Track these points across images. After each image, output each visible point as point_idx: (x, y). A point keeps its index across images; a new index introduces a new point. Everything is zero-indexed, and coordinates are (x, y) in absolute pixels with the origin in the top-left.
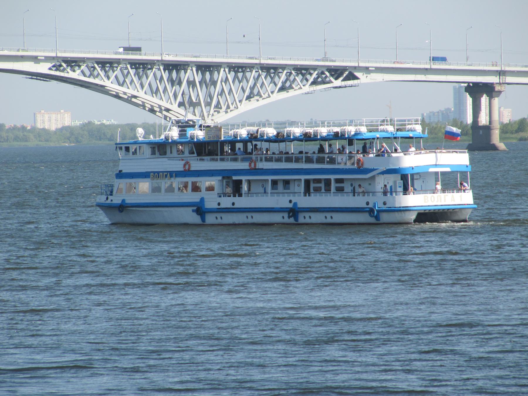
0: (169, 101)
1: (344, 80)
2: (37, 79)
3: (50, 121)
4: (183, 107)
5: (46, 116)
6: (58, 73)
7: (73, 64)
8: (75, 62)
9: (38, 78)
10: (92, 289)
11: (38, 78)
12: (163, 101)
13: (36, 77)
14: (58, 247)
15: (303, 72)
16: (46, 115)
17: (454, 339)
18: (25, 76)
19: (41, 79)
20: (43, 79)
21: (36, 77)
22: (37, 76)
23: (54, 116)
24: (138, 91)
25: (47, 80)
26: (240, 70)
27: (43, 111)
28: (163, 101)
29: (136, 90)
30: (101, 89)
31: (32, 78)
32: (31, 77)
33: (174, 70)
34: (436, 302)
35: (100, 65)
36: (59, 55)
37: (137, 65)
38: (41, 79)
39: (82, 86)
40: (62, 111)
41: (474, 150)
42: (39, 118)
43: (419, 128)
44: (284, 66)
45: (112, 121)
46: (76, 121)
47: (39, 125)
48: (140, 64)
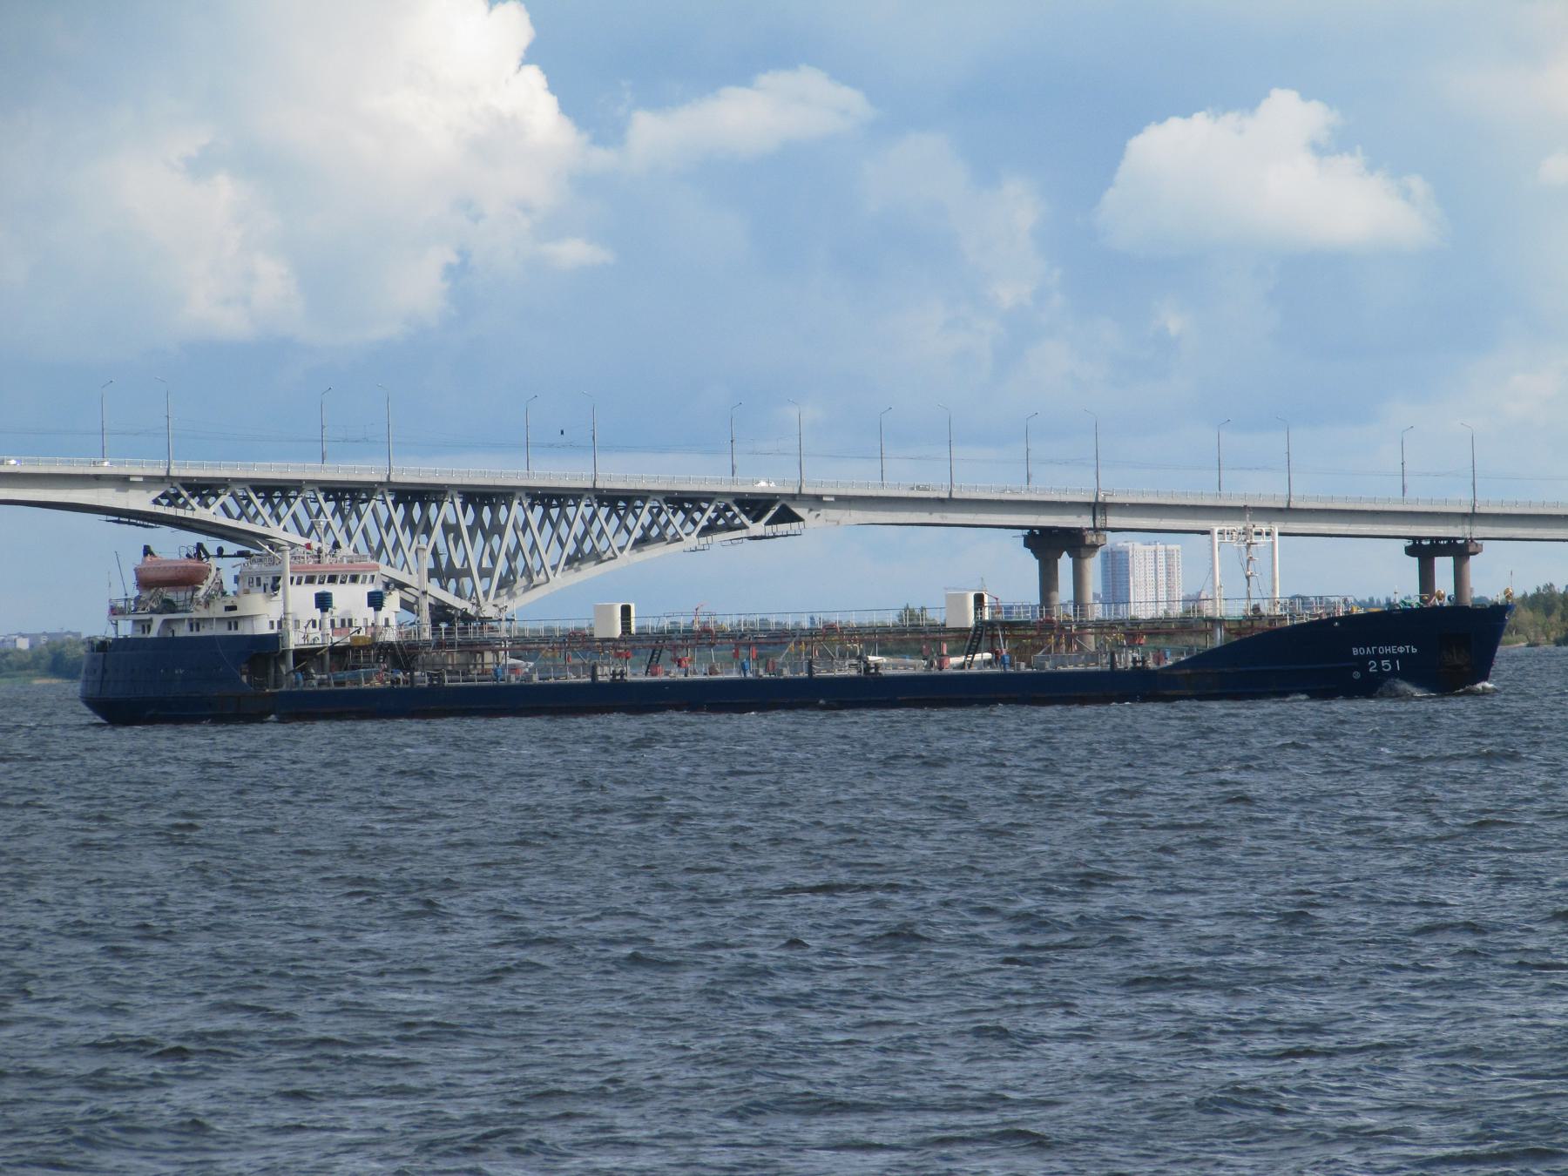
2: (129, 523)
6: (171, 511)
15: (687, 505)
18: (104, 517)
26: (554, 502)
31: (118, 522)
33: (417, 504)
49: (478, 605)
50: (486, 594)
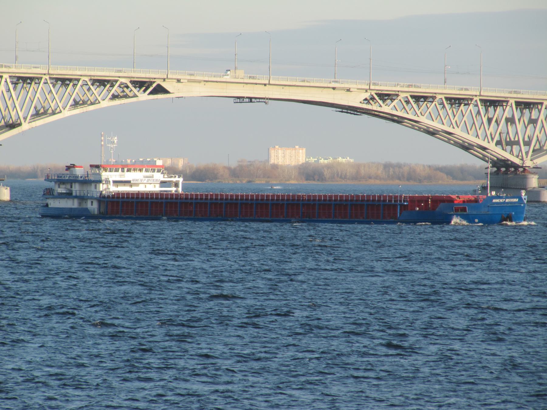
0: (486, 139)
1: (151, 93)
2: (347, 113)
3: (284, 157)
4: (500, 146)
5: (280, 152)
6: (369, 107)
7: (386, 98)
8: (388, 95)
9: (349, 111)
10: (190, 316)
11: (349, 111)
12: (479, 138)
13: (346, 111)
14: (226, 274)
16: (280, 151)
17: (538, 316)
18: (335, 109)
19: (352, 112)
20: (350, 111)
21: (346, 111)
22: (347, 109)
23: (288, 152)
24: (454, 128)
25: (358, 113)
27: (277, 147)
28: (479, 138)
29: (452, 126)
30: (415, 124)
31: (342, 112)
32: (341, 110)
34: (470, 321)
35: (414, 100)
36: (51, 72)
37: (453, 101)
38: (352, 112)
39: (394, 121)
40: (297, 147)
41: (415, 223)
42: (273, 153)
43: (95, 205)
44: (471, 97)
45: (348, 158)
46: (311, 158)
47: (273, 161)
48: (456, 99)
49: (522, 159)
50: (527, 153)
